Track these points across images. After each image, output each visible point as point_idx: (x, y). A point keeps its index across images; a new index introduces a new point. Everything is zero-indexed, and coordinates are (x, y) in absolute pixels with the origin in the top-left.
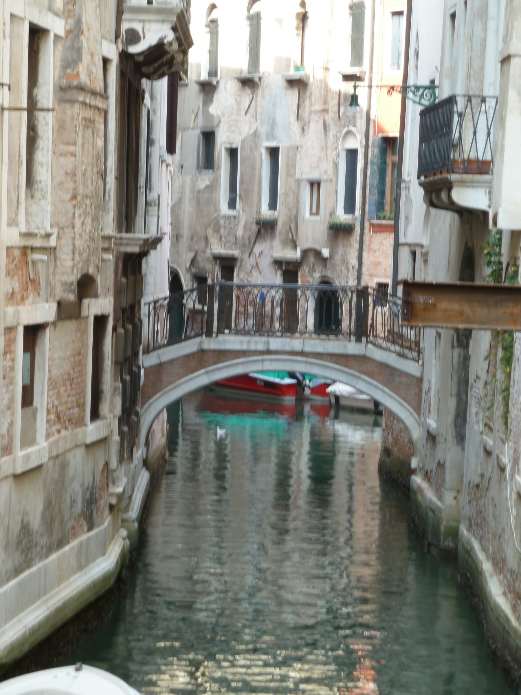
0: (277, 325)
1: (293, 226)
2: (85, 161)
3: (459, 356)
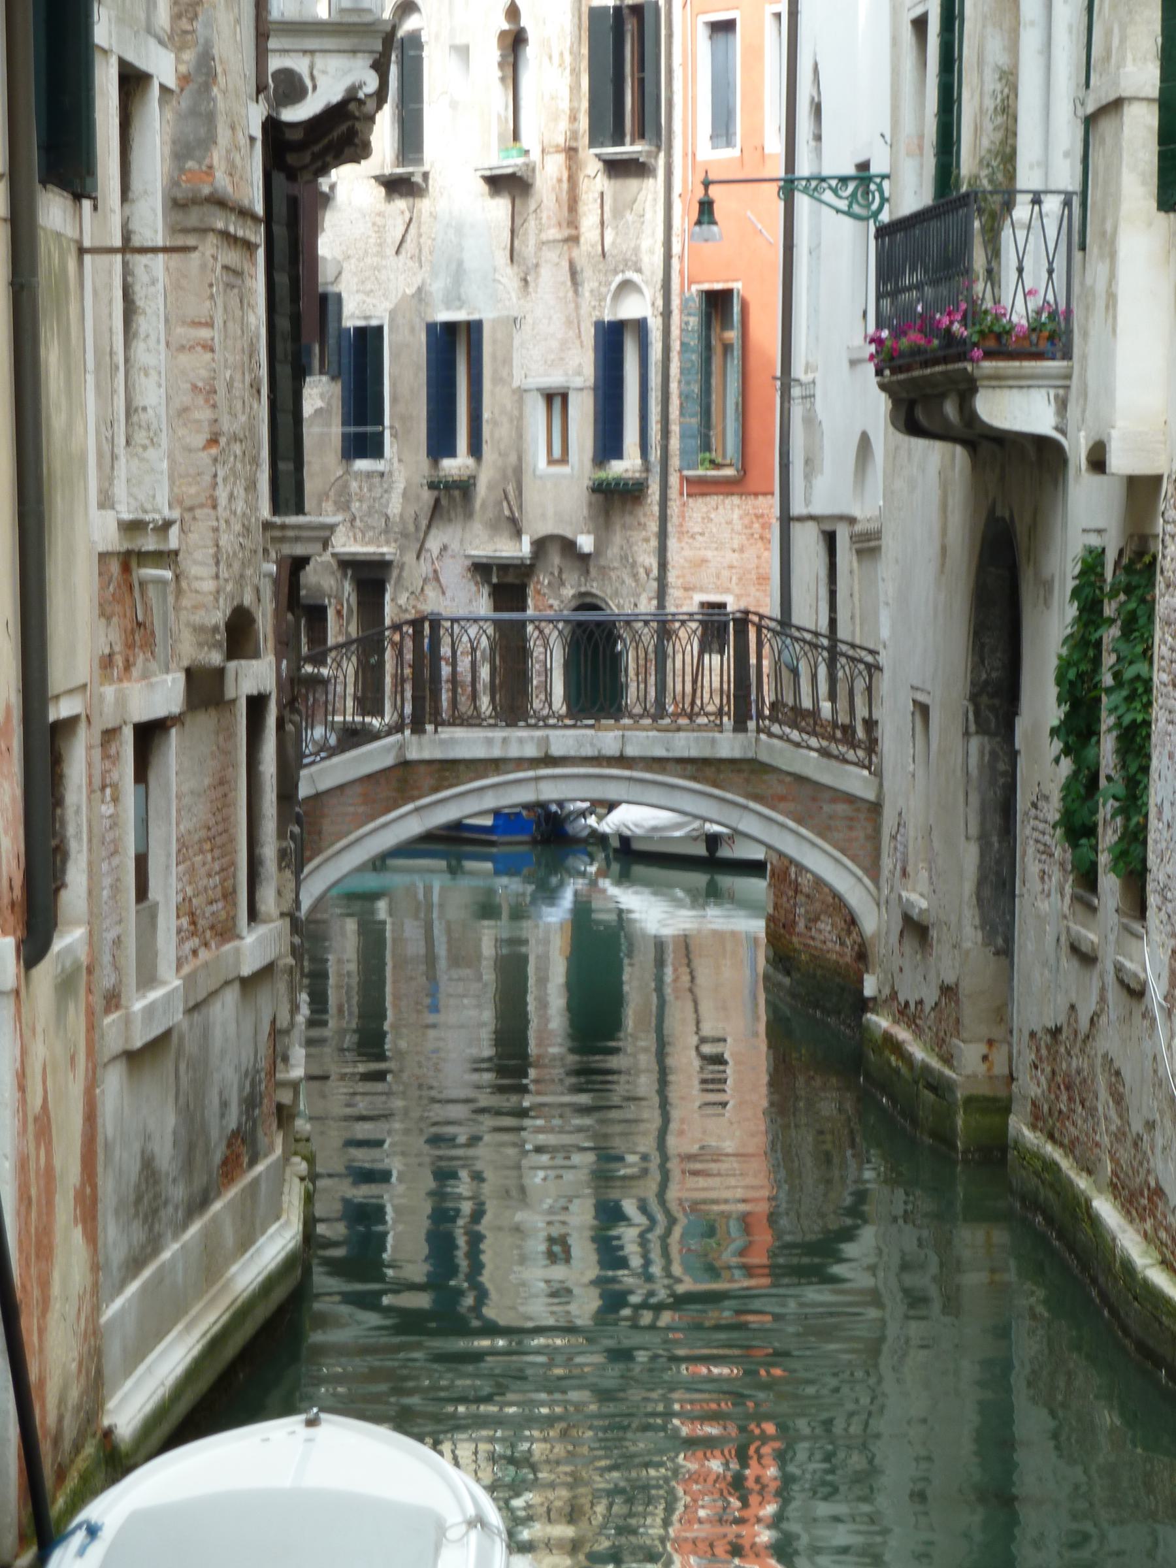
0: (485, 702)
1: (511, 489)
2: (231, 360)
3: (982, 753)
